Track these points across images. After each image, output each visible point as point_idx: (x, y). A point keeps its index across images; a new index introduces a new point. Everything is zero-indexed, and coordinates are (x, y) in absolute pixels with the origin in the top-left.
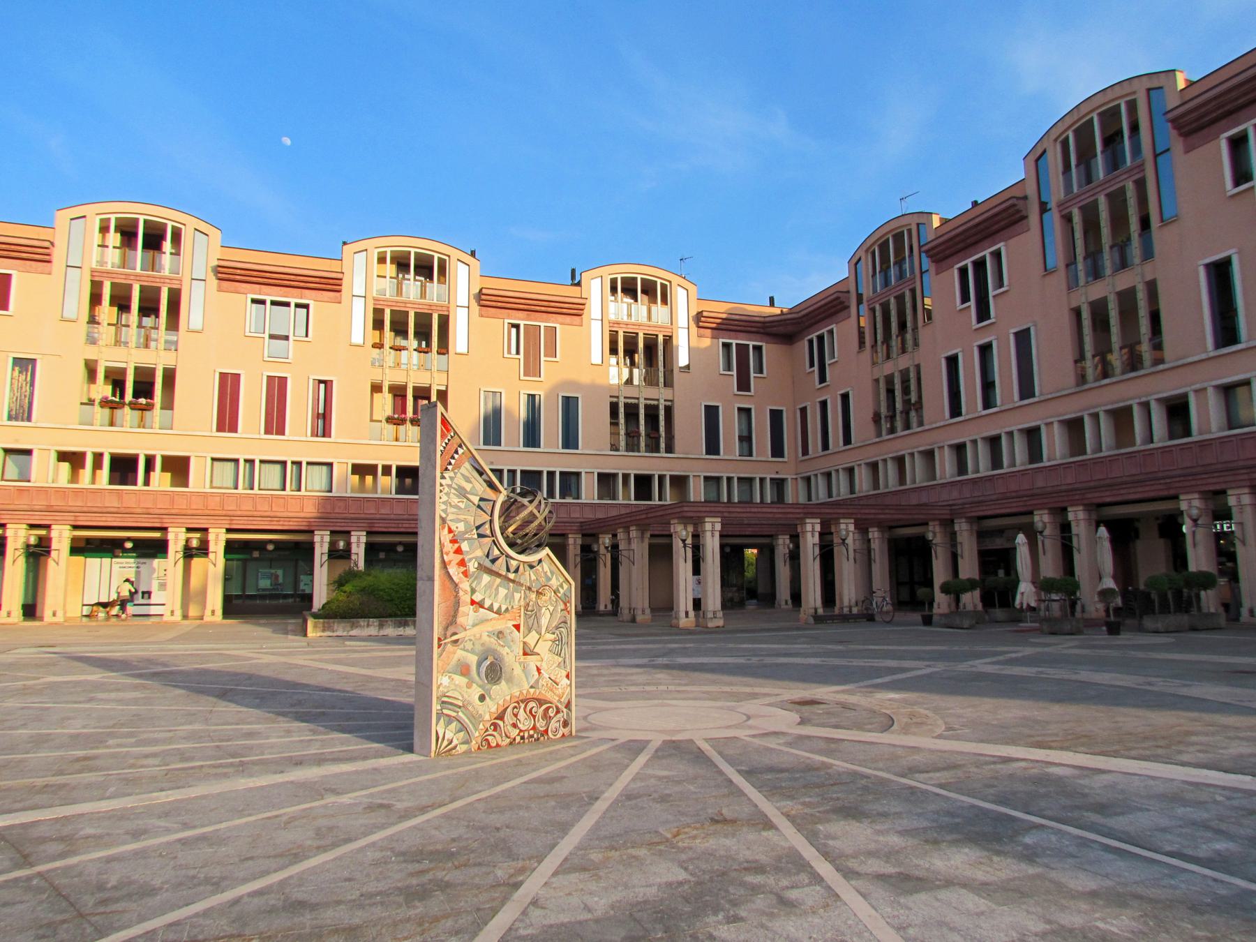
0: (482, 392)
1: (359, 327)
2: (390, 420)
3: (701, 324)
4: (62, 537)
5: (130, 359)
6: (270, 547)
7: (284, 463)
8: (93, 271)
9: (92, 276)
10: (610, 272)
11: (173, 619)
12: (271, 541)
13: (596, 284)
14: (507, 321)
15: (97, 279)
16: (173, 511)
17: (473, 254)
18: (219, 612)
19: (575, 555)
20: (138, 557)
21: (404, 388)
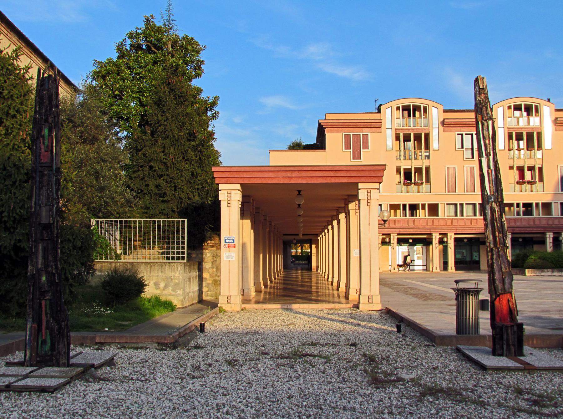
0: (559, 167)
1: (390, 141)
2: (517, 183)
3: (557, 124)
4: (394, 238)
5: (412, 164)
6: (465, 240)
7: (456, 205)
8: (396, 129)
9: (396, 131)
10: (507, 103)
11: (394, 271)
12: (465, 238)
13: (389, 111)
14: (344, 134)
15: (398, 132)
16: (434, 227)
17: (549, 100)
18: (454, 268)
19: (550, 242)
20: (409, 246)
21: (523, 167)
